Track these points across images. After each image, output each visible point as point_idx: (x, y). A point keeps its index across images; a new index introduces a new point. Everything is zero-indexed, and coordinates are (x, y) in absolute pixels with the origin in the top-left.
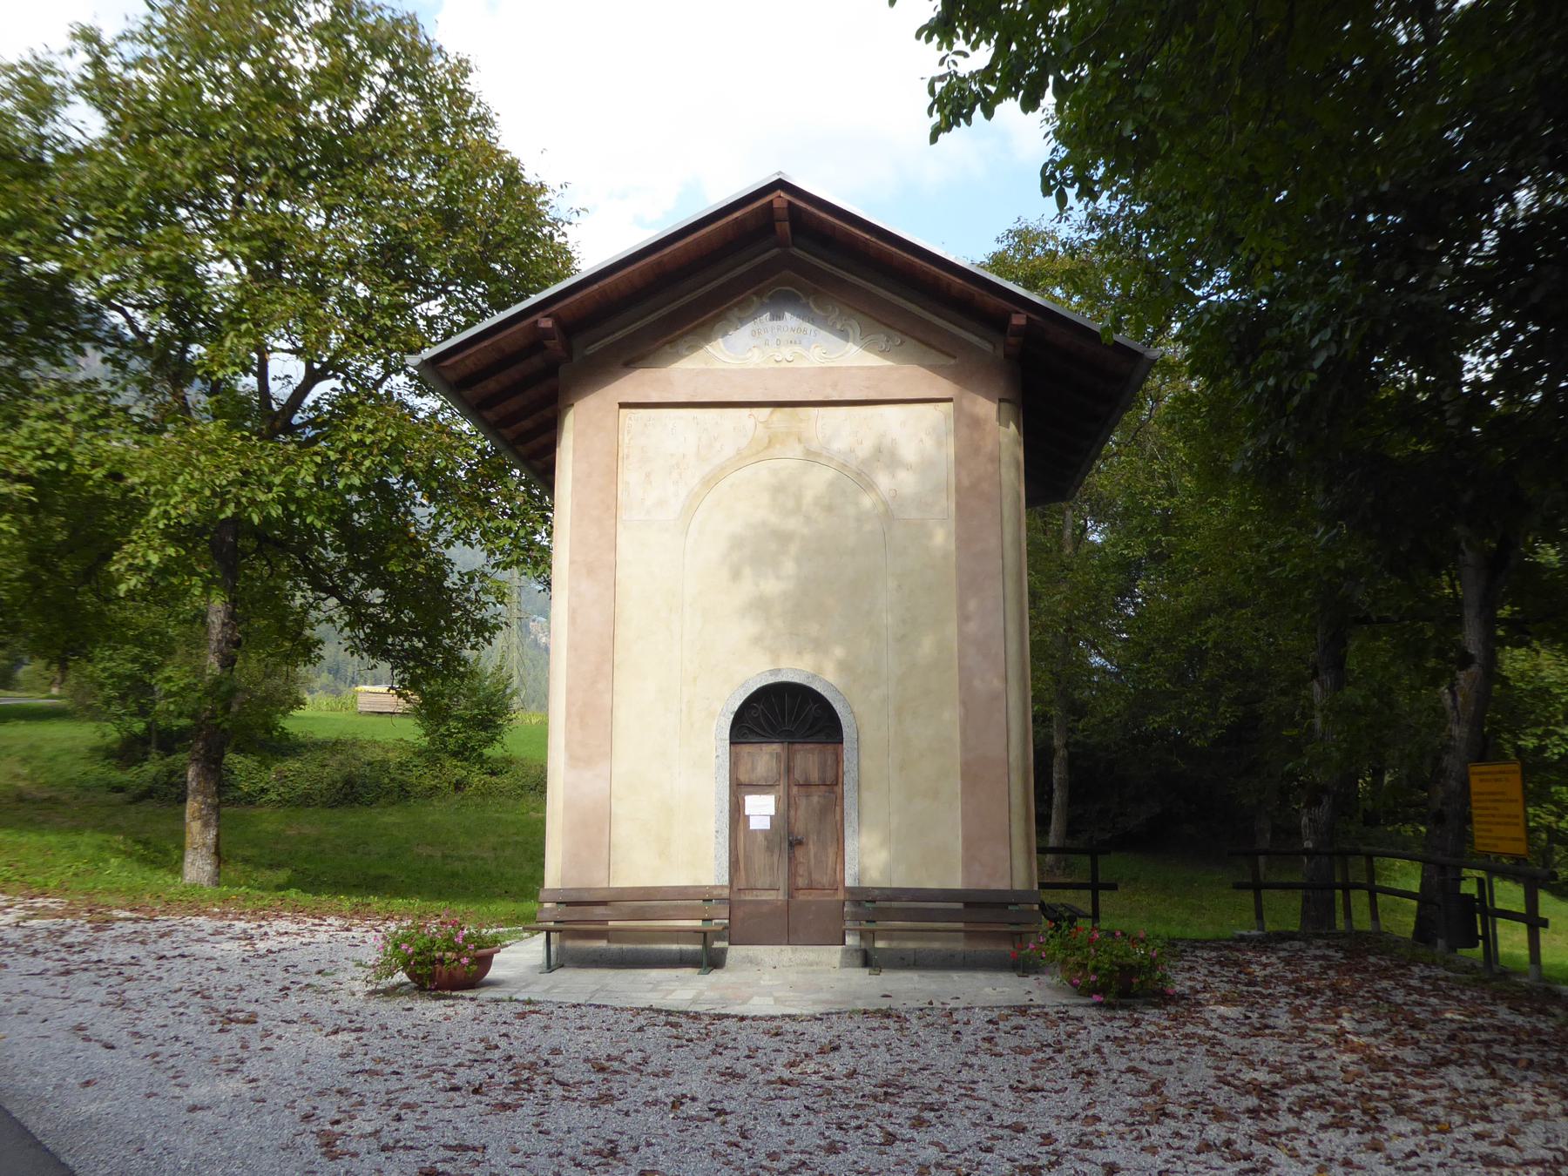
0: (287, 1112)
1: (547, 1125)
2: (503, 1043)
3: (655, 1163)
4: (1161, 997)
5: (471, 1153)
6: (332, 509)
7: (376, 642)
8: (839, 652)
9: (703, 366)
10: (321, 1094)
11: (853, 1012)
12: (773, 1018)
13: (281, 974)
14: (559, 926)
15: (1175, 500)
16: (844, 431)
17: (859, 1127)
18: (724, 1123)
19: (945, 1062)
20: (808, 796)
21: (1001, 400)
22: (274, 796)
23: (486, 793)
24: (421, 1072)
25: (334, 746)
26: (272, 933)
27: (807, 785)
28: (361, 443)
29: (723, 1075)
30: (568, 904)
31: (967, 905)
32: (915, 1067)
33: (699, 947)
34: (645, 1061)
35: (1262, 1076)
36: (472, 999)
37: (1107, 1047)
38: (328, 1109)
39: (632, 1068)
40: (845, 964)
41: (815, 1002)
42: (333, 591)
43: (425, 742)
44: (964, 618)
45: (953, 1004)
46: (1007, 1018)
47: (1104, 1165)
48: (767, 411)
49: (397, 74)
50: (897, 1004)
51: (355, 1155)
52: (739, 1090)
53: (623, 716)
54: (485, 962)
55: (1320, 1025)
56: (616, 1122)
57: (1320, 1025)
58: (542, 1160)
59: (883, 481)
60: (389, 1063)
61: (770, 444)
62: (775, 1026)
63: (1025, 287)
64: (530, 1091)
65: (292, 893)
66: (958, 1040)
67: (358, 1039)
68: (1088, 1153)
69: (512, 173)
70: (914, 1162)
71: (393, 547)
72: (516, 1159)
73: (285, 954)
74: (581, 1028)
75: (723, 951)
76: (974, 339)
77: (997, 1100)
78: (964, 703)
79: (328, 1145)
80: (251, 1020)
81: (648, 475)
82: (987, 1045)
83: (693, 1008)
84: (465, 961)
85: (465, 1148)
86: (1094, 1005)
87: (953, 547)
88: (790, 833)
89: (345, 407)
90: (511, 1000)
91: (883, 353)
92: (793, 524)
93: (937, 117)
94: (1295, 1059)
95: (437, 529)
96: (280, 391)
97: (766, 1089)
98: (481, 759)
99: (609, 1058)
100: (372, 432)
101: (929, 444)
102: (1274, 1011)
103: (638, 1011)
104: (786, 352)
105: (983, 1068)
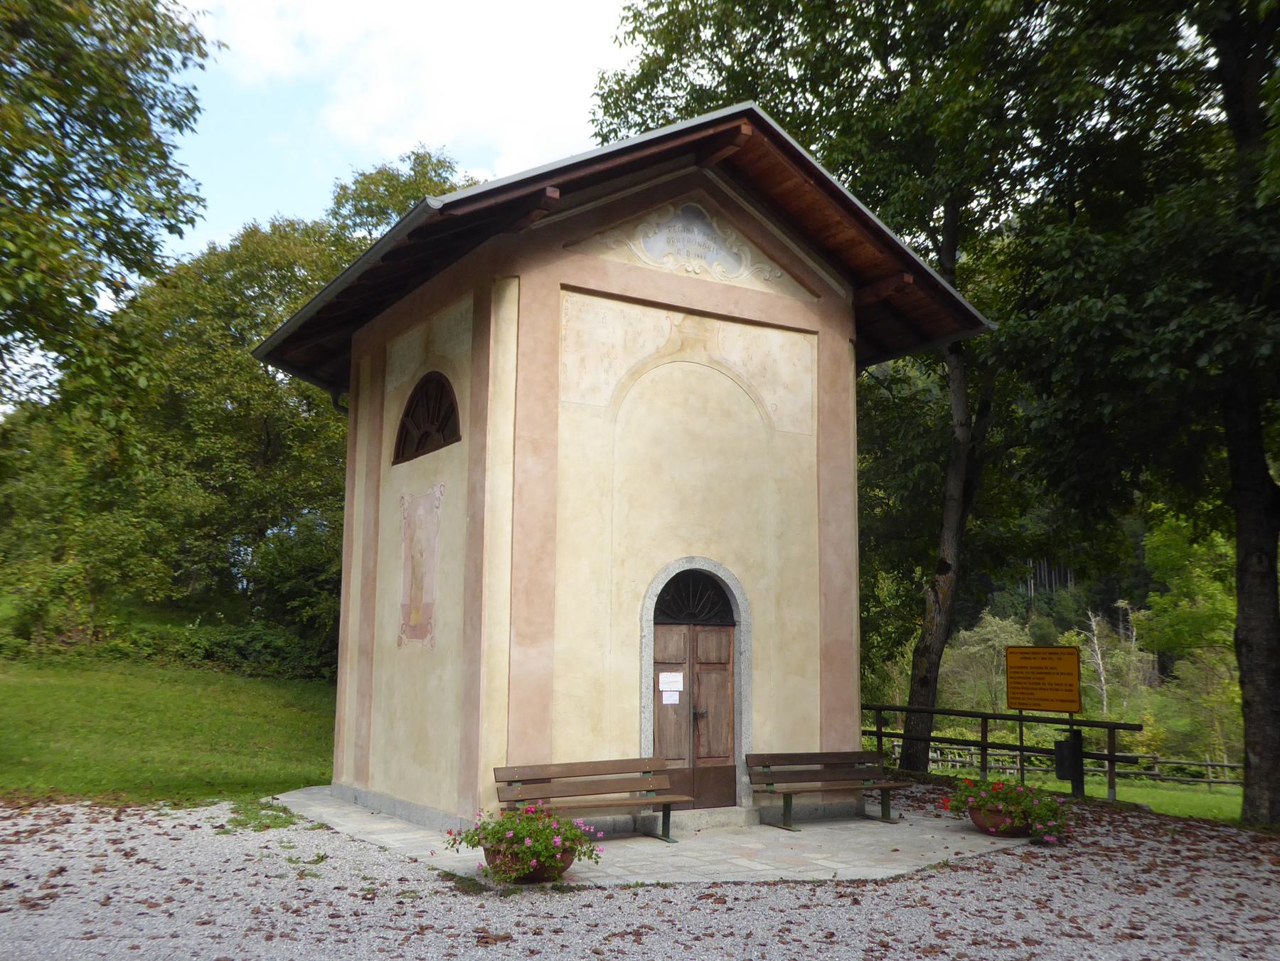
16: (733, 342)
30: (524, 782)
31: (826, 766)
48: (679, 317)
61: (681, 349)
81: (583, 360)
104: (695, 264)
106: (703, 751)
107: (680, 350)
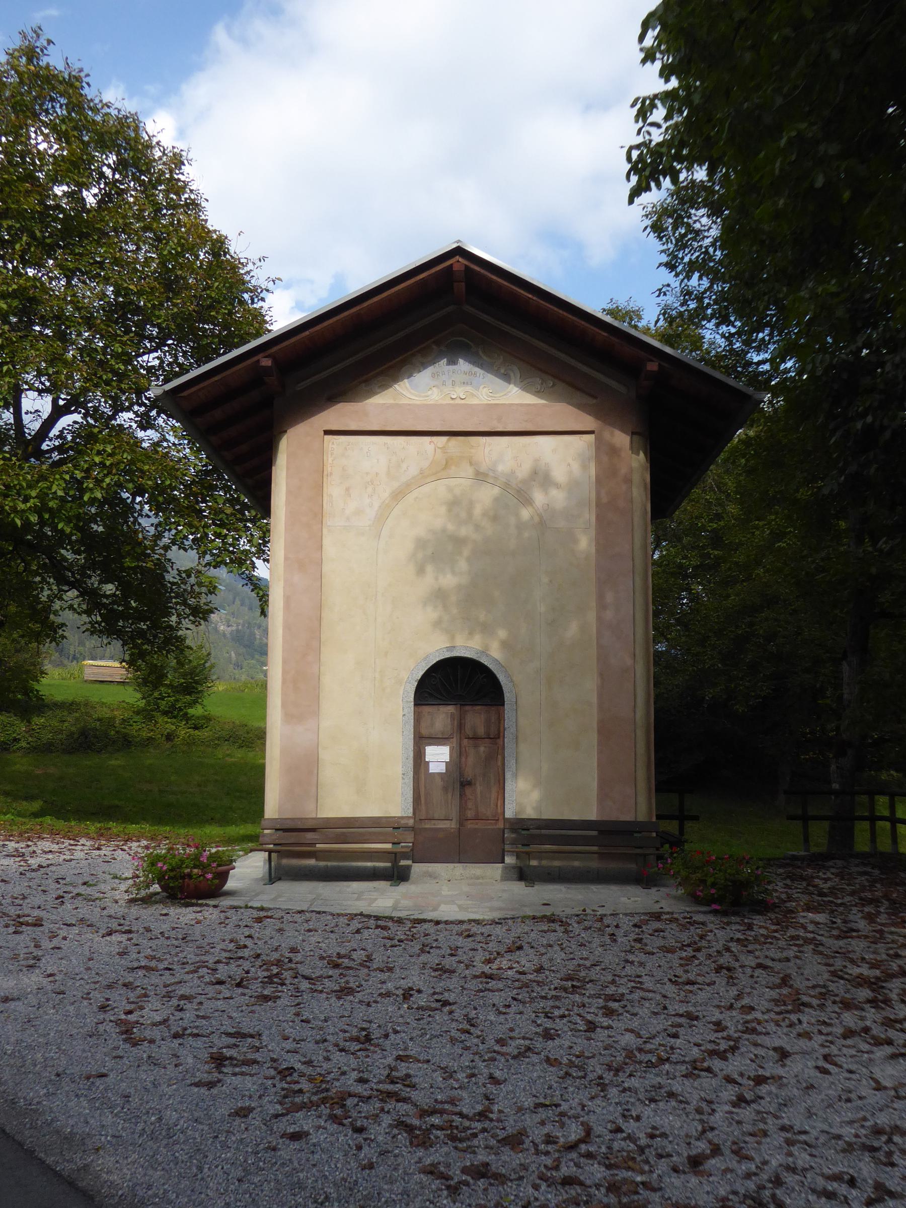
0: (85, 1003)
1: (306, 1015)
2: (249, 942)
3: (406, 1049)
4: (762, 907)
5: (250, 1040)
6: (78, 517)
7: (109, 624)
8: (502, 634)
9: (392, 401)
10: (109, 987)
11: (524, 917)
12: (461, 922)
13: (54, 886)
14: (279, 848)
15: (722, 523)
16: (504, 455)
17: (563, 1017)
18: (451, 1012)
19: (611, 958)
20: (476, 746)
21: (633, 433)
22: (24, 744)
23: (190, 743)
24: (188, 968)
25: (70, 706)
26: (39, 852)
27: (475, 738)
28: (102, 464)
29: (436, 970)
32: (588, 963)
33: (389, 864)
34: (369, 958)
35: (865, 970)
36: (215, 906)
37: (734, 947)
38: (120, 1000)
39: (361, 965)
40: (505, 878)
41: (492, 909)
42: (73, 585)
43: (142, 704)
44: (602, 606)
45: (601, 911)
46: (646, 922)
47: (775, 1049)
48: (444, 439)
49: (121, 166)
50: (558, 911)
51: (152, 1041)
52: (453, 982)
53: (327, 681)
54: (223, 877)
55: (893, 929)
56: (361, 1013)
57: (893, 929)
58: (311, 1045)
59: (539, 498)
60: (160, 960)
61: (447, 466)
62: (466, 929)
63: (660, 341)
64: (283, 984)
65: (48, 820)
66: (615, 941)
67: (130, 939)
68: (760, 1039)
69: (219, 246)
70: (618, 1047)
71: (128, 548)
72: (289, 1045)
73: (53, 868)
74: (309, 931)
75: (409, 868)
76: (613, 384)
77: (664, 992)
78: (601, 675)
79: (127, 1031)
80: (38, 923)
81: (348, 489)
82: (638, 945)
83: (396, 914)
84: (210, 876)
85: (244, 1036)
86: (710, 912)
87: (593, 550)
88: (461, 774)
89: (86, 437)
90: (246, 907)
91: (538, 393)
92: (464, 531)
93: (634, 179)
94: (884, 957)
95: (159, 536)
96: (32, 425)
97: (474, 982)
98: (186, 717)
99: (339, 956)
100: (110, 455)
101: (576, 467)
102: (851, 917)
103: (352, 917)
104: (460, 392)
105: (641, 964)
106: (470, 814)
107: (443, 469)
